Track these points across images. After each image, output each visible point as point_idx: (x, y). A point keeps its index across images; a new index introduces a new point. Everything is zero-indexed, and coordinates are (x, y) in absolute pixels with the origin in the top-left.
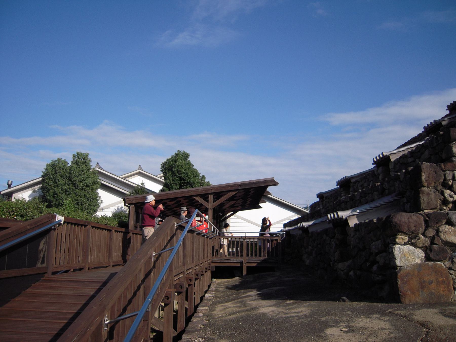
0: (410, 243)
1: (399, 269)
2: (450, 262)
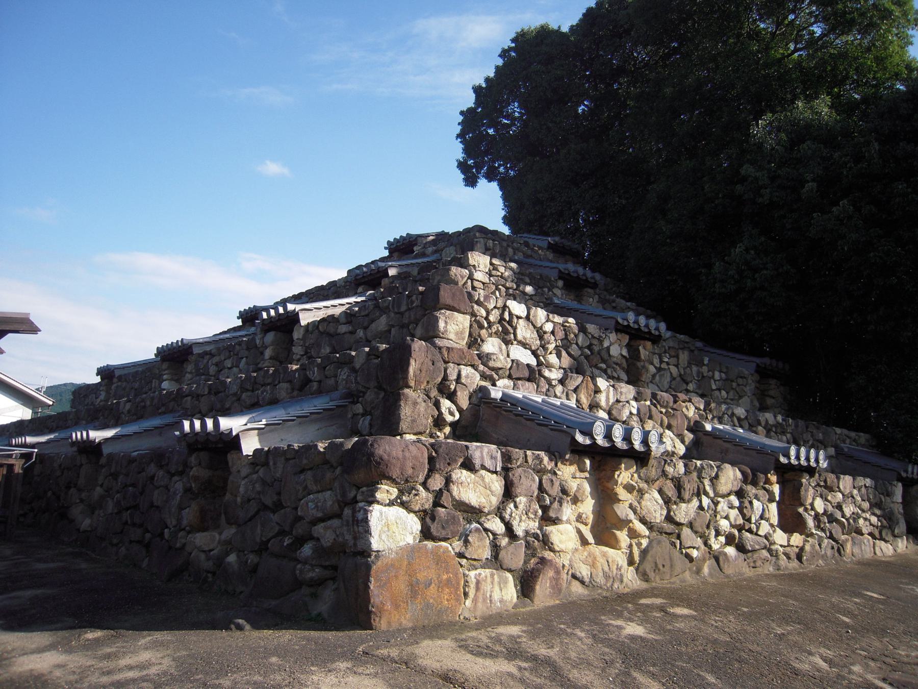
0: (399, 501)
1: (376, 555)
2: (461, 543)
